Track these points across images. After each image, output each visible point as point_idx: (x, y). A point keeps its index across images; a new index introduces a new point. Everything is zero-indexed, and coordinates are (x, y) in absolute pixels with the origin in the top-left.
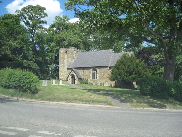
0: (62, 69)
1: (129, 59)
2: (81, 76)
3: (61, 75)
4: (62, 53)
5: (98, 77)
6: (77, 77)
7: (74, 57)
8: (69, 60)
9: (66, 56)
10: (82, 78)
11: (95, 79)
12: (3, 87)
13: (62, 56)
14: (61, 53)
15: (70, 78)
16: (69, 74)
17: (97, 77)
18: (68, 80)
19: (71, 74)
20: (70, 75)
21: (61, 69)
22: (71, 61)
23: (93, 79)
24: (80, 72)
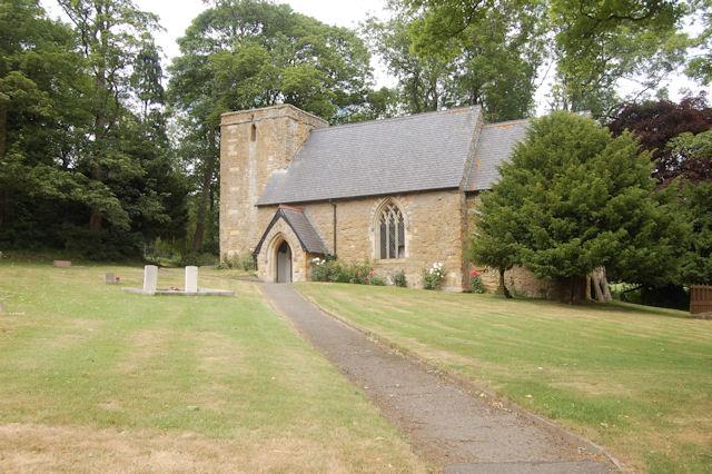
0: (236, 211)
2: (326, 242)
5: (407, 244)
8: (269, 167)
9: (252, 147)
11: (392, 256)
13: (231, 148)
14: (229, 133)
16: (264, 237)
17: (402, 247)
18: (260, 266)
19: (273, 232)
20: (269, 237)
21: (232, 212)
22: (276, 171)
24: (320, 219)
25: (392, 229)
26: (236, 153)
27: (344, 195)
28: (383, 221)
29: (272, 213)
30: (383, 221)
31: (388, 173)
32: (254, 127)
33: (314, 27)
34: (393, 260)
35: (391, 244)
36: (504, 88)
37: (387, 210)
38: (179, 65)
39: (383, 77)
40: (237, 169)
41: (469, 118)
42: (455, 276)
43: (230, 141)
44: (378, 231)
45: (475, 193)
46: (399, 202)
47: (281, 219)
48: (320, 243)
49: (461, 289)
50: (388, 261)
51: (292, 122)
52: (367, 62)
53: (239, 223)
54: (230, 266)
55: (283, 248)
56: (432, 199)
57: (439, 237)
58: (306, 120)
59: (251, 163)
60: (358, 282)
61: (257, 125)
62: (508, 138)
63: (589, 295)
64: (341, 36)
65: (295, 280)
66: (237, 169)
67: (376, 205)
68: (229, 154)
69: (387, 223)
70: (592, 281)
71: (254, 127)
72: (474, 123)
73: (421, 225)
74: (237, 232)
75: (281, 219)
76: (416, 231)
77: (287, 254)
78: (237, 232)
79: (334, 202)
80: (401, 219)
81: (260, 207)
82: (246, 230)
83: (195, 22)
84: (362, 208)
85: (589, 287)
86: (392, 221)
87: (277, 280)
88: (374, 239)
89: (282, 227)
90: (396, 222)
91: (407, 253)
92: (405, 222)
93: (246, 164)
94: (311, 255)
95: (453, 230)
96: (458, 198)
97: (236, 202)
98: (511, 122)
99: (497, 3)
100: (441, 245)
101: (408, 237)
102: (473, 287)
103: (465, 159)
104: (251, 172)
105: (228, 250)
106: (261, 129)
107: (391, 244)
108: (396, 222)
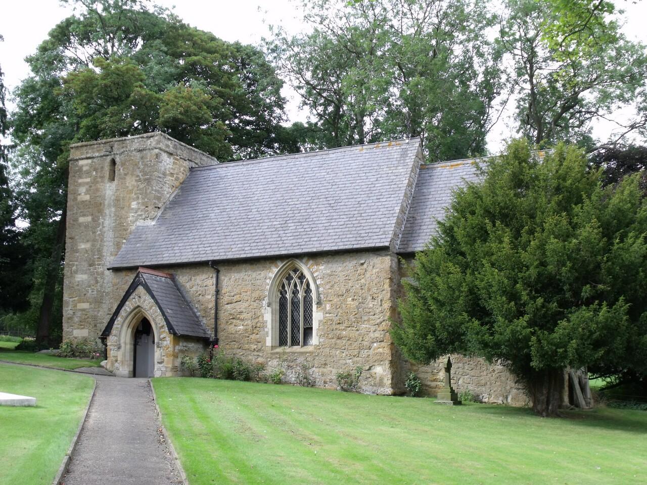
0: (85, 277)
1: (554, 183)
2: (204, 321)
3: (76, 319)
4: (88, 173)
5: (315, 326)
6: (170, 328)
7: (159, 198)
8: (131, 216)
9: (109, 190)
10: (211, 334)
11: (295, 342)
12: (111, 271)
13: (82, 190)
14: (80, 170)
15: (122, 336)
16: (117, 313)
17: (308, 331)
18: (112, 353)
19: (129, 306)
20: (123, 313)
21: (81, 277)
22: (140, 223)
23: (282, 342)
24: (199, 285)
25: (295, 304)
26: (87, 197)
27: (230, 256)
28: (283, 293)
29: (130, 278)
30: (283, 293)
31: (292, 226)
32: (113, 162)
33: (205, 44)
34: (296, 348)
35: (293, 325)
36: (454, 123)
37: (289, 278)
38: (28, 90)
39: (296, 112)
40: (89, 219)
41: (404, 154)
42: (382, 371)
43: (80, 181)
44: (276, 306)
45: (120, 18)
46: (305, 268)
47: (141, 289)
48: (196, 322)
49: (389, 391)
50: (288, 349)
51: (164, 156)
52: (276, 92)
53: (86, 288)
54: (74, 355)
55: (142, 330)
56: (348, 266)
57: (357, 310)
58: (185, 154)
59: (107, 211)
60: (247, 379)
61: (118, 160)
62: (455, 178)
63: (566, 399)
64: (243, 57)
65: (157, 374)
66: (89, 219)
67: (273, 271)
68: (79, 198)
69: (289, 296)
70: (570, 379)
71: (113, 162)
72: (411, 159)
73: (336, 300)
74: (85, 306)
75: (140, 288)
76: (328, 307)
77: (150, 337)
78: (85, 306)
79: (217, 266)
80: (308, 290)
81: (116, 270)
82: (98, 301)
83: (52, 34)
84: (254, 275)
85: (566, 388)
86: (295, 292)
87: (134, 374)
88: (269, 317)
89: (142, 300)
90: (301, 295)
91: (315, 340)
92: (314, 295)
93: (101, 211)
94: (178, 338)
95: (380, 304)
96: (384, 263)
97: (85, 264)
98: (459, 162)
99: (646, 80)
100: (364, 326)
101: (317, 316)
102: (407, 387)
103: (397, 209)
104: (108, 222)
105: (75, 332)
106: (123, 164)
107: (293, 325)
108: (301, 295)
